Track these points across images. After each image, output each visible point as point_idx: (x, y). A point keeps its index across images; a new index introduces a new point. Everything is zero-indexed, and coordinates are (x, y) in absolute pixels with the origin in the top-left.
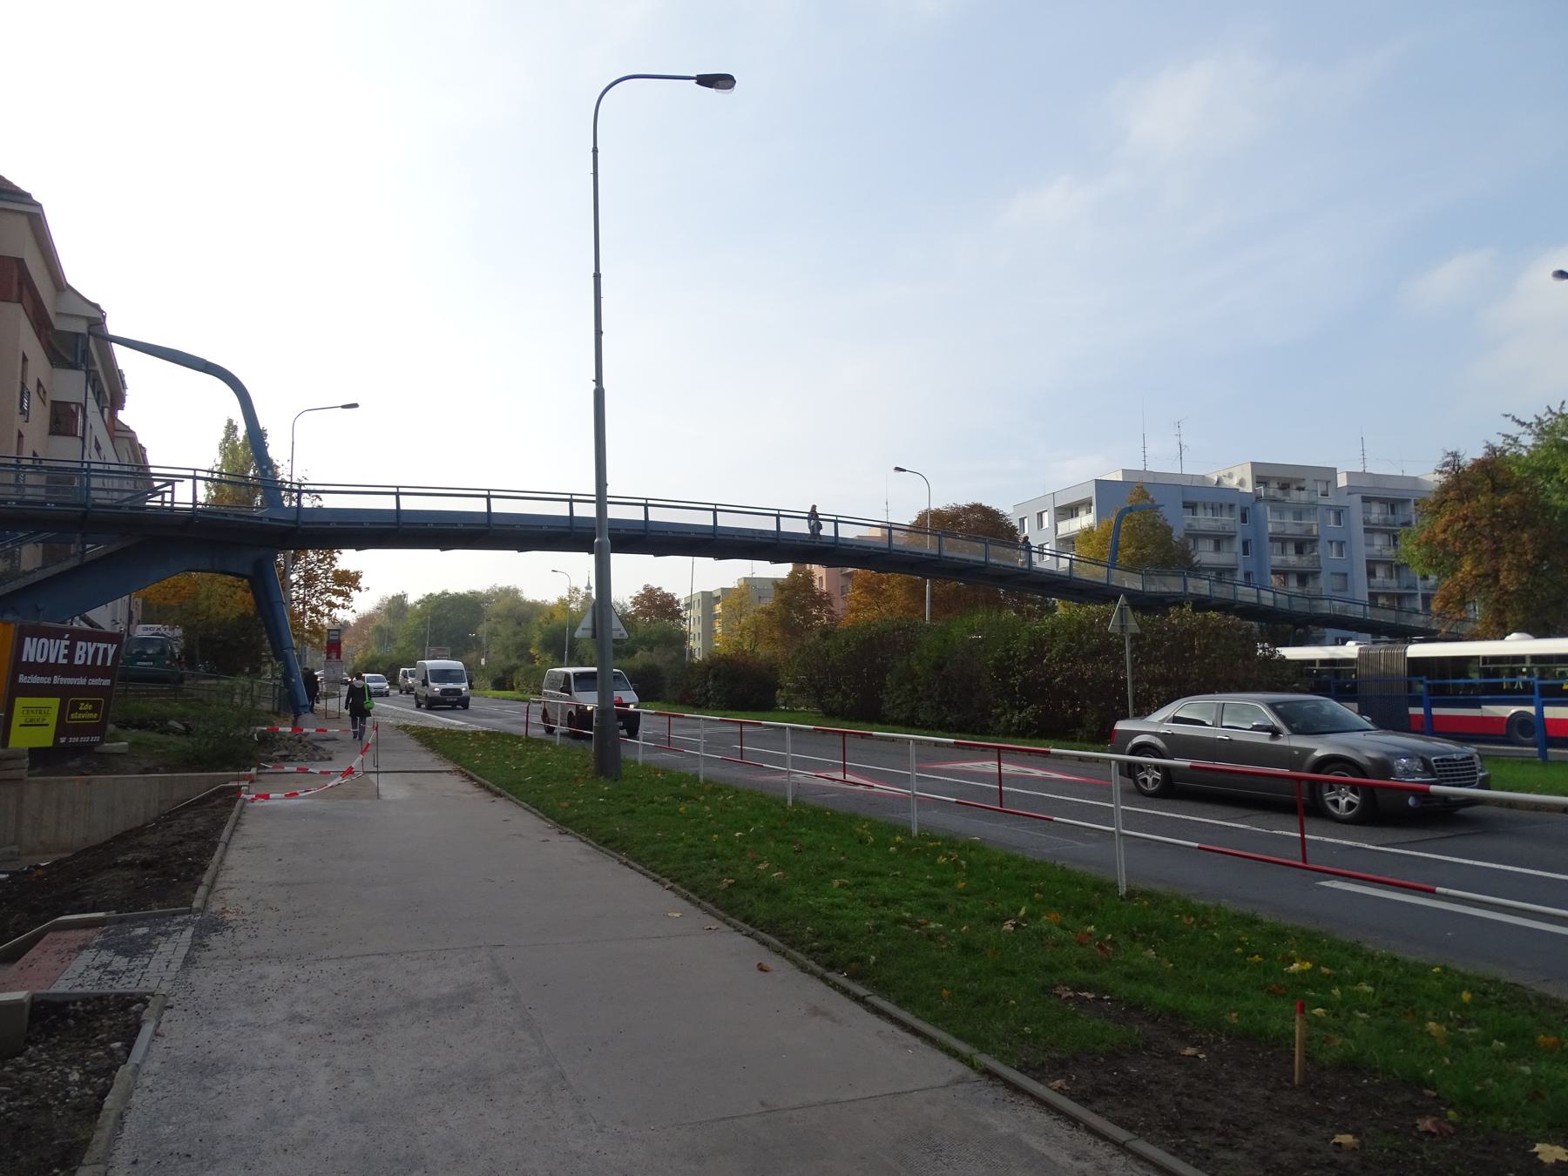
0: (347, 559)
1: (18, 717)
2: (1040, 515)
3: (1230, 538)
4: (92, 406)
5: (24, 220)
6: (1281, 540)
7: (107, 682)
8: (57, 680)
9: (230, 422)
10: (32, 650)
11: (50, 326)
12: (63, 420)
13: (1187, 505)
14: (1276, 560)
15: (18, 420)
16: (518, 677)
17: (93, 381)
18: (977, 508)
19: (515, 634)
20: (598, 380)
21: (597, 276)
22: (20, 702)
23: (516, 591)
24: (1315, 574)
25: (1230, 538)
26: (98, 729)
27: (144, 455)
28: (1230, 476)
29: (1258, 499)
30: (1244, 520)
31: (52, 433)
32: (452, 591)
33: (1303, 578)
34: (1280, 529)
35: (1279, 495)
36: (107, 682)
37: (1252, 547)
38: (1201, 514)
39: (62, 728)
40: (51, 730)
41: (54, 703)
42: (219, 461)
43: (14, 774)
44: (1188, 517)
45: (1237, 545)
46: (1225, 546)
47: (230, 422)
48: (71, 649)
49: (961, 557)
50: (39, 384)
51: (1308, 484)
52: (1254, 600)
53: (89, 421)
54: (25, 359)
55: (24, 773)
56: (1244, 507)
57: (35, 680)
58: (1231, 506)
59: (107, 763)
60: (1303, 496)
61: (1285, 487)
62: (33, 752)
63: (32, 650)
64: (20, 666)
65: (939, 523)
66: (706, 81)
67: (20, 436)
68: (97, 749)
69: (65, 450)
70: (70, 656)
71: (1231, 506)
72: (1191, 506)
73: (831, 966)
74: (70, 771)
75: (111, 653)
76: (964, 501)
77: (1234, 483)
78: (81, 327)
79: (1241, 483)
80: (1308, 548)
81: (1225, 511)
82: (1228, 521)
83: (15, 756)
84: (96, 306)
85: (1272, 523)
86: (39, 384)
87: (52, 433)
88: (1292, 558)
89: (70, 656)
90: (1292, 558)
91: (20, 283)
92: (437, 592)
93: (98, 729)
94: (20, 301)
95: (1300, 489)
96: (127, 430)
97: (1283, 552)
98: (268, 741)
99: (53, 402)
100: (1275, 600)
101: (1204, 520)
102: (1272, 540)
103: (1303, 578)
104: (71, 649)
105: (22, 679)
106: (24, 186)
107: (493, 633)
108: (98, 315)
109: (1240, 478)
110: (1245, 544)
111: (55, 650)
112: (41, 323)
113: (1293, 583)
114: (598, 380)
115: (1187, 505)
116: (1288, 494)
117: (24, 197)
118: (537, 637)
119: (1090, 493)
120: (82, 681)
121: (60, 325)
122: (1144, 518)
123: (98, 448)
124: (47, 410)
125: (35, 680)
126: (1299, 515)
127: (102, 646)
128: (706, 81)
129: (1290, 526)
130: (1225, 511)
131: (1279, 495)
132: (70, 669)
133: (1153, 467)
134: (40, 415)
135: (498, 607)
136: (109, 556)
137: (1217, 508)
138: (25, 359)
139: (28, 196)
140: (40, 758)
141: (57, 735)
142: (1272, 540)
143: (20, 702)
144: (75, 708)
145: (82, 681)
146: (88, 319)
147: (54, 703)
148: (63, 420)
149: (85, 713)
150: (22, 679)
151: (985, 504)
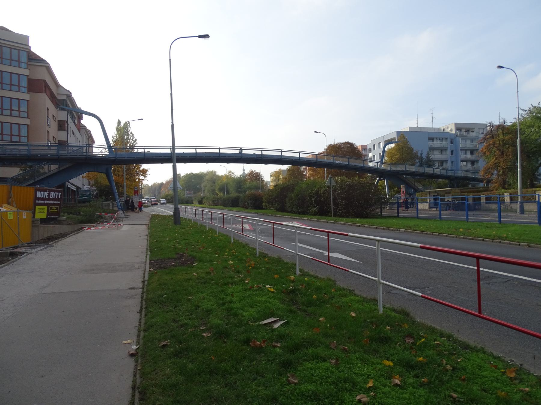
0: (144, 166)
1: (37, 211)
2: (380, 143)
3: (446, 150)
4: (70, 121)
5: (44, 69)
6: (465, 150)
7: (59, 202)
8: (46, 202)
9: (119, 121)
10: (39, 194)
11: (55, 98)
12: (61, 126)
13: (430, 139)
14: (463, 157)
15: (47, 128)
16: (204, 200)
17: (70, 112)
18: (347, 143)
19: (212, 186)
20: (172, 122)
21: (171, 94)
22: (37, 207)
23: (215, 172)
24: (477, 161)
25: (446, 150)
26: (58, 214)
27: (90, 133)
28: (448, 128)
29: (457, 136)
30: (452, 143)
31: (59, 130)
32: (194, 173)
33: (473, 163)
34: (464, 146)
35: (465, 134)
36: (59, 202)
37: (454, 153)
38: (435, 142)
39: (48, 214)
40: (45, 214)
41: (46, 207)
42: (116, 133)
43: (37, 224)
44: (431, 143)
45: (449, 152)
46: (444, 152)
47: (119, 121)
48: (49, 194)
49: (344, 158)
50: (53, 116)
51: (476, 130)
52: (432, 172)
53: (69, 126)
54: (48, 109)
55: (39, 224)
56: (452, 139)
57: (41, 202)
58: (446, 139)
59: (60, 222)
60: (474, 134)
61: (468, 131)
62: (41, 219)
63: (39, 194)
64: (36, 199)
65: (335, 150)
66: (201, 37)
67: (48, 132)
68: (58, 219)
69: (62, 136)
70: (49, 196)
71: (446, 139)
72: (432, 139)
73: (150, 252)
74: (51, 224)
75: (60, 195)
76: (342, 140)
77: (448, 130)
78: (64, 98)
79: (451, 130)
80: (475, 152)
81: (444, 140)
82: (446, 144)
83: (37, 220)
84: (69, 91)
85: (461, 144)
86: (53, 116)
87: (59, 130)
88: (469, 156)
89: (49, 196)
90: (469, 156)
91: (45, 87)
92: (189, 172)
93: (58, 214)
94: (46, 93)
95: (473, 132)
96: (84, 126)
97: (466, 154)
98: (100, 217)
99: (58, 121)
100: (440, 172)
101: (437, 144)
102: (461, 150)
103: (473, 163)
104: (49, 194)
105: (37, 202)
106: (44, 57)
107: (205, 186)
108: (69, 94)
109: (451, 129)
110: (452, 151)
111: (45, 194)
112: (52, 97)
113: (469, 165)
114: (172, 122)
115: (430, 139)
116: (469, 134)
117: (44, 61)
118: (217, 187)
119: (395, 136)
120: (52, 202)
121: (59, 97)
122: (405, 145)
123: (73, 133)
124: (57, 123)
125: (41, 202)
126: (472, 141)
127: (57, 193)
128: (201, 37)
129: (469, 144)
130: (444, 140)
131: (465, 134)
132: (49, 199)
133: (420, 125)
134: (54, 125)
135: (207, 177)
136: (67, 168)
137: (442, 139)
138: (48, 109)
139: (45, 61)
140: (43, 221)
141: (47, 215)
142: (461, 150)
143: (37, 207)
144: (51, 208)
145: (52, 202)
146: (67, 95)
147: (46, 207)
148: (61, 126)
149: (54, 210)
150: (37, 202)
151: (350, 142)
